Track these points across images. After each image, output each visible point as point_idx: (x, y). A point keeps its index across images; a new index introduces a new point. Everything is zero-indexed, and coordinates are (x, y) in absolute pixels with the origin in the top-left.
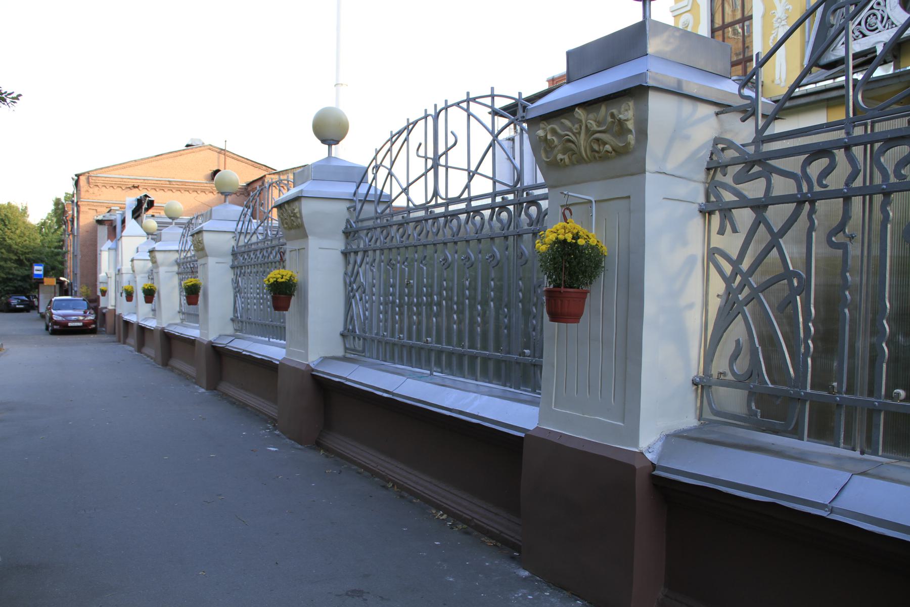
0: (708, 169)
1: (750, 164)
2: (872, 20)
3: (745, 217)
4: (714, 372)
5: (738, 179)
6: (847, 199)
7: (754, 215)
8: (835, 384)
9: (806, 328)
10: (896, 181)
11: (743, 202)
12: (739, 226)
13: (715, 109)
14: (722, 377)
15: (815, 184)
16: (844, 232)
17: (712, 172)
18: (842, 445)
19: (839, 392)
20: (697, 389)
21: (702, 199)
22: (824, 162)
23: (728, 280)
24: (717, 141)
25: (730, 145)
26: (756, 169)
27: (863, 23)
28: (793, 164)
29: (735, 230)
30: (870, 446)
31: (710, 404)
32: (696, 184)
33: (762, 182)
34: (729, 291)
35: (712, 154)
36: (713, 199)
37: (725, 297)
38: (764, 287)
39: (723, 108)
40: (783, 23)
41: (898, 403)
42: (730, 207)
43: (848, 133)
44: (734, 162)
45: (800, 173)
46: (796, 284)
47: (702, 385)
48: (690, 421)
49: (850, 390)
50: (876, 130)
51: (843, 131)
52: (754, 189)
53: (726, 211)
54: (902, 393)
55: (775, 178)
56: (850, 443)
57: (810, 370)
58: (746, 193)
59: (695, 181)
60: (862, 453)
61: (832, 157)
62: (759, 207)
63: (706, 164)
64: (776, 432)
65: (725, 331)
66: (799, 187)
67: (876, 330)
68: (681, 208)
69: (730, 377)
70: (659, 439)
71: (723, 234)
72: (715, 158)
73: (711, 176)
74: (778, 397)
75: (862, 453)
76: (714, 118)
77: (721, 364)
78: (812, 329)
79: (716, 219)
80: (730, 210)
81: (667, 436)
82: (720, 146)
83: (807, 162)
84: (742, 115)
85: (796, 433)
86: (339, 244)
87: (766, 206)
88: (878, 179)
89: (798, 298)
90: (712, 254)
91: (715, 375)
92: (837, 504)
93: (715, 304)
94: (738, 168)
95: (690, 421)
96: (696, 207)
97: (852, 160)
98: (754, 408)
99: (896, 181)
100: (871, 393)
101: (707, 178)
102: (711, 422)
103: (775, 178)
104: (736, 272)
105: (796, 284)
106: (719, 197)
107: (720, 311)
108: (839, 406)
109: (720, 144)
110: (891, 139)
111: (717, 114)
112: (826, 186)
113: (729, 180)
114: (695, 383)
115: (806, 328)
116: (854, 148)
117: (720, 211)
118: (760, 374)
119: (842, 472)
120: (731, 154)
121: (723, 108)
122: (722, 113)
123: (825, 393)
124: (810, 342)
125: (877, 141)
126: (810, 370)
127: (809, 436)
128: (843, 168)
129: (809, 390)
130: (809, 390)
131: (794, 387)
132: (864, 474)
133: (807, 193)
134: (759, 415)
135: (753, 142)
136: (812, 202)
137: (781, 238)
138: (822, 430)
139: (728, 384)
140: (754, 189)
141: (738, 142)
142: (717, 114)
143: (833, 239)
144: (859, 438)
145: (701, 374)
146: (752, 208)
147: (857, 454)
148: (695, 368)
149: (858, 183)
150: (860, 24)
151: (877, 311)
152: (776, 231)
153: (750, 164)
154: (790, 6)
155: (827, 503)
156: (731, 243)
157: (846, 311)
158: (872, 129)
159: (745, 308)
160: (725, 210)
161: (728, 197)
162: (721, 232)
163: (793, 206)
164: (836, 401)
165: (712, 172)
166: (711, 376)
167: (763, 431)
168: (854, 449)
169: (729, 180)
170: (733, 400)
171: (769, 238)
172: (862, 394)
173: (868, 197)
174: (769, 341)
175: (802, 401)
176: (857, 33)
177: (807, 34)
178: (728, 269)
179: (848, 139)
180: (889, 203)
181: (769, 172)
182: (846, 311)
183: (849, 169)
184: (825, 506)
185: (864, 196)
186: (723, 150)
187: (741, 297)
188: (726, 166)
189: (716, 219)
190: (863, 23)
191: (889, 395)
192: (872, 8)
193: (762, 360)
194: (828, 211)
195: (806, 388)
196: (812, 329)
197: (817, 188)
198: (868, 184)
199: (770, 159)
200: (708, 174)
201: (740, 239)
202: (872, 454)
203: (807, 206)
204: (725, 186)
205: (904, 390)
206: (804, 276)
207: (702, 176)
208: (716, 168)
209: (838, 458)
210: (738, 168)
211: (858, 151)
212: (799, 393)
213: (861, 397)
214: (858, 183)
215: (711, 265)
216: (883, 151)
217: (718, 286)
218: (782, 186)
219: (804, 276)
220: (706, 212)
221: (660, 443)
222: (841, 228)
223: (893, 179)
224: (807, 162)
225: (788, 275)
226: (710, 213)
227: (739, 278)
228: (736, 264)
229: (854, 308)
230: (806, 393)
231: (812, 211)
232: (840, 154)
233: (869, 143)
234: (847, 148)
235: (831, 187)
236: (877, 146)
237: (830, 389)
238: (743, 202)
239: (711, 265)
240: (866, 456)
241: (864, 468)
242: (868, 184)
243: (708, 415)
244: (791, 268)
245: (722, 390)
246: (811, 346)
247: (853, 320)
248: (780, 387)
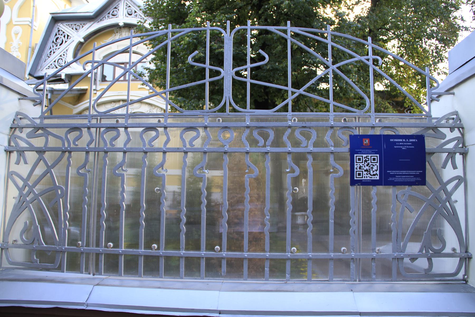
0: (11, 128)
1: (37, 128)
2: (60, 61)
3: (32, 156)
4: (10, 241)
5: (29, 136)
6: (87, 152)
8: (80, 242)
9: (65, 216)
11: (32, 148)
13: (19, 96)
18: (84, 272)
21: (6, 144)
22: (77, 133)
23: (21, 190)
24: (18, 114)
25: (26, 117)
26: (40, 132)
27: (56, 61)
28: (61, 132)
29: (26, 163)
30: (97, 271)
31: (7, 259)
35: (14, 120)
36: (12, 144)
37: (18, 199)
39: (23, 96)
40: (17, 50)
41: (110, 249)
43: (89, 122)
44: (27, 127)
46: (60, 193)
49: (88, 245)
50: (102, 122)
51: (87, 120)
53: (21, 152)
54: (111, 244)
55: (50, 138)
56: (87, 271)
57: (67, 236)
59: (3, 134)
60: (94, 275)
62: (41, 152)
63: (10, 125)
64: (48, 270)
66: (64, 144)
67: (99, 216)
69: (20, 242)
73: (12, 132)
75: (94, 275)
76: (17, 101)
78: (68, 215)
79: (14, 156)
80: (23, 151)
82: (19, 117)
84: (33, 103)
85: (60, 269)
87: (45, 152)
88: (102, 145)
90: (10, 175)
92: (89, 302)
93: (12, 202)
94: (30, 130)
97: (90, 134)
98: (35, 258)
100: (98, 245)
103: (50, 138)
105: (60, 193)
106: (17, 144)
107: (15, 207)
108: (82, 253)
109: (20, 116)
110: (109, 127)
111: (19, 99)
112: (77, 145)
113: (24, 135)
115: (65, 216)
116: (91, 129)
117: (17, 151)
118: (39, 240)
119: (88, 286)
120: (26, 122)
121: (23, 96)
122: (22, 99)
123: (75, 247)
124: (67, 222)
125: (103, 127)
127: (66, 270)
129: (66, 247)
130: (66, 247)
131: (59, 245)
132: (98, 285)
134: (38, 261)
135: (40, 118)
136: (70, 152)
138: (74, 266)
139: (19, 247)
140: (38, 142)
142: (19, 99)
144: (92, 267)
146: (36, 151)
147: (91, 276)
149: (92, 146)
150: (55, 61)
151: (100, 205)
152: (50, 165)
153: (38, 129)
154: (21, 43)
155: (85, 302)
156: (24, 170)
157: (86, 206)
158: (100, 122)
160: (21, 151)
161: (23, 145)
162: (18, 163)
165: (13, 130)
167: (41, 270)
168: (89, 274)
169: (24, 135)
171: (46, 168)
172: (93, 247)
173: (97, 153)
174: (44, 222)
175: (63, 252)
176: (53, 66)
177: (28, 59)
178: (21, 183)
179: (90, 124)
180: (107, 156)
181: (47, 134)
182: (86, 206)
183: (89, 139)
184: (84, 303)
185: (95, 152)
186: (21, 119)
187: (28, 199)
188: (23, 128)
190: (56, 61)
191: (106, 246)
192: (61, 56)
193: (40, 232)
194: (78, 157)
196: (68, 215)
197: (72, 146)
198: (97, 146)
199: (48, 128)
200: (11, 131)
202: (99, 275)
203: (67, 154)
204: (21, 138)
205: (155, 244)
206: (64, 189)
207: (7, 131)
208: (16, 128)
209: (82, 279)
210: (30, 130)
211: (93, 130)
213: (93, 248)
214: (92, 146)
215: (10, 180)
216: (105, 132)
217: (14, 192)
218: (52, 143)
219: (64, 189)
220: (9, 152)
222: (84, 166)
226: (10, 152)
228: (25, 181)
229: (89, 205)
230: (65, 248)
231: (70, 157)
232: (85, 130)
233: (98, 127)
234: (89, 128)
235: (80, 146)
236: (102, 129)
238: (32, 148)
240: (95, 276)
241: (97, 282)
242: (97, 146)
244: (57, 185)
245: (15, 250)
246: (68, 224)
247: (89, 211)
248: (49, 246)
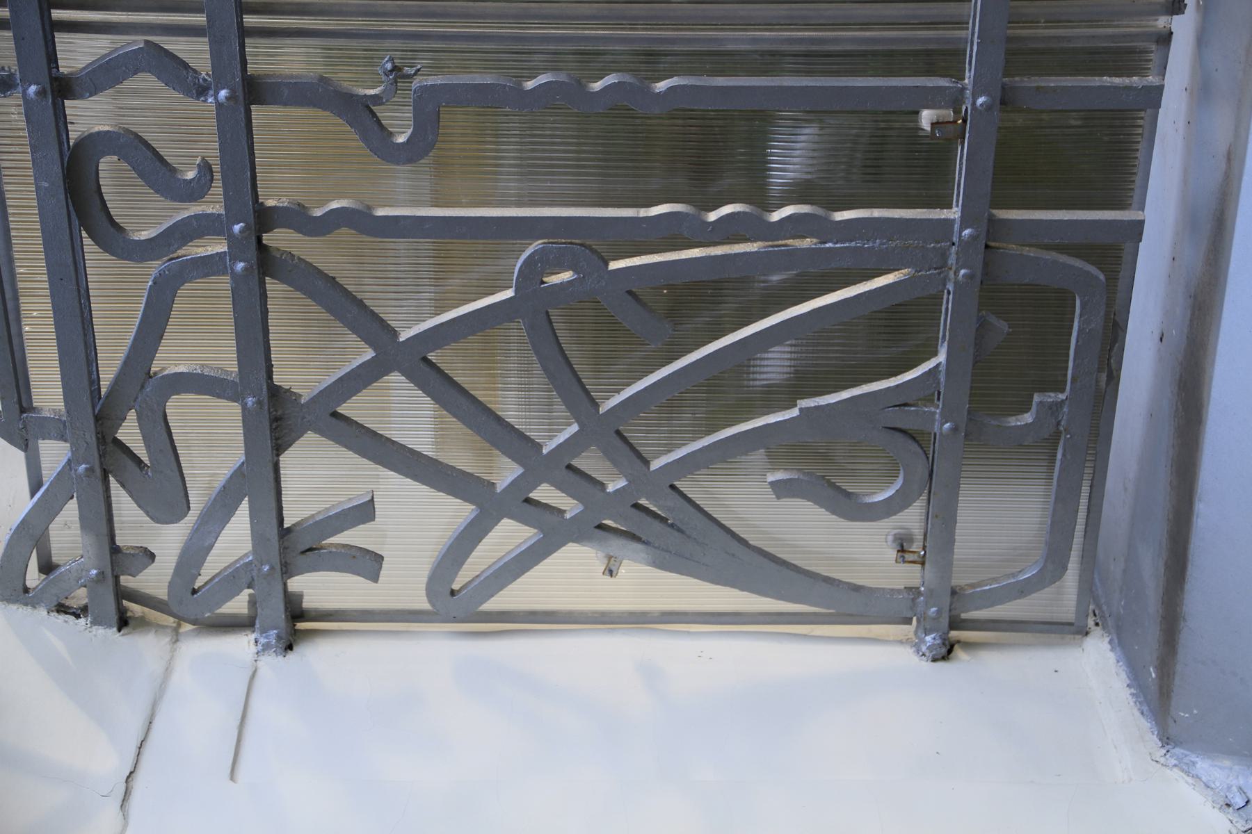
0: (123, 622)
1: (107, 459)
3: (315, 477)
5: (167, 499)
6: (254, 90)
7: (310, 437)
8: (927, 117)
9: (729, 230)
10: (217, 189)
11: (260, 480)
12: (352, 495)
14: (916, 546)
15: (195, 209)
16: (377, 99)
17: (135, 609)
18: (1152, 79)
19: (955, 101)
20: (969, 646)
21: (242, 645)
22: (110, 173)
23: (554, 533)
26: (130, 432)
29: (364, 512)
31: (1023, 590)
32: (182, 677)
33: (180, 409)
34: (594, 529)
35: (62, 609)
36: (238, 605)
37: (617, 545)
38: (579, 399)
42: (273, 533)
44: (101, 521)
45: (154, 267)
47: (952, 626)
48: (1095, 665)
52: (211, 439)
53: (291, 547)
57: (877, 213)
58: (224, 473)
61: (94, 145)
62: (277, 421)
63: (100, 631)
65: (744, 542)
66: (208, 266)
68: (269, 711)
69: (912, 518)
70: (1187, 769)
71: (379, 558)
72: (80, 596)
74: (982, 325)
77: (868, 551)
78: (727, 209)
79: (317, 588)
80: (284, 532)
81: (1167, 740)
82: (33, 577)
83: (112, 236)
85: (1113, 254)
86: (210, 669)
87: (276, 393)
89: (614, 265)
90: (457, 602)
91: (909, 575)
93: (642, 582)
94: (124, 505)
95: (1095, 665)
96: (272, 664)
97: (106, 75)
99: (217, 189)
101: (159, 627)
102: (1087, 588)
104: (523, 505)
105: (567, 276)
106: (231, 580)
108: (1006, 100)
112: (206, 168)
113: (168, 541)
114: (946, 652)
115: (729, 230)
117: (287, 570)
118: (901, 400)
120: (67, 533)
123: (962, 153)
126: (877, 213)
127: (1121, 205)
128: (142, 105)
129: (954, 213)
130: (954, 213)
131: (943, 266)
133: (231, 238)
134: (1052, 397)
135: (25, 444)
136: (264, 219)
137: (395, 334)
139: (943, 521)
140: (211, 439)
141: (22, 503)
143: (401, 139)
145: (908, 630)
148: (889, 656)
149: (195, 53)
152: (369, 354)
156: (413, 524)
157: (661, 86)
159: (656, 465)
160: (284, 550)
161: (236, 539)
162: (368, 563)
163: (274, 287)
164: (988, 107)
165: (135, 609)
166: (913, 591)
167: (1113, 378)
168: (1165, 38)
169: (168, 541)
170: (999, 519)
175: (993, 236)
178: (509, 535)
179: (27, 82)
181: (143, 385)
182: (661, 86)
185: (245, 32)
186: (47, 567)
188: (115, 550)
189: (317, 588)
194: (297, 160)
195: (949, 223)
196: (727, 209)
197: (213, 205)
198: (200, 19)
199: (95, 382)
200: (143, 624)
201: (396, 492)
203: (277, 239)
207: (146, 647)
208: (122, 594)
212: (965, 245)
214: (195, 53)
217: (573, 574)
218: (200, 341)
220: (295, 625)
221: (1203, 766)
222: (360, 113)
223: (213, 205)
224: (112, 236)
225: (534, 310)
226: (296, 612)
227: (545, 493)
228: (490, 506)
229: (652, 60)
230: (965, 222)
231: (297, 218)
232: (87, 116)
235: (212, 151)
237: (948, 134)
238: (260, 480)
239: (494, 604)
243: (1064, 596)
244: (509, 293)
